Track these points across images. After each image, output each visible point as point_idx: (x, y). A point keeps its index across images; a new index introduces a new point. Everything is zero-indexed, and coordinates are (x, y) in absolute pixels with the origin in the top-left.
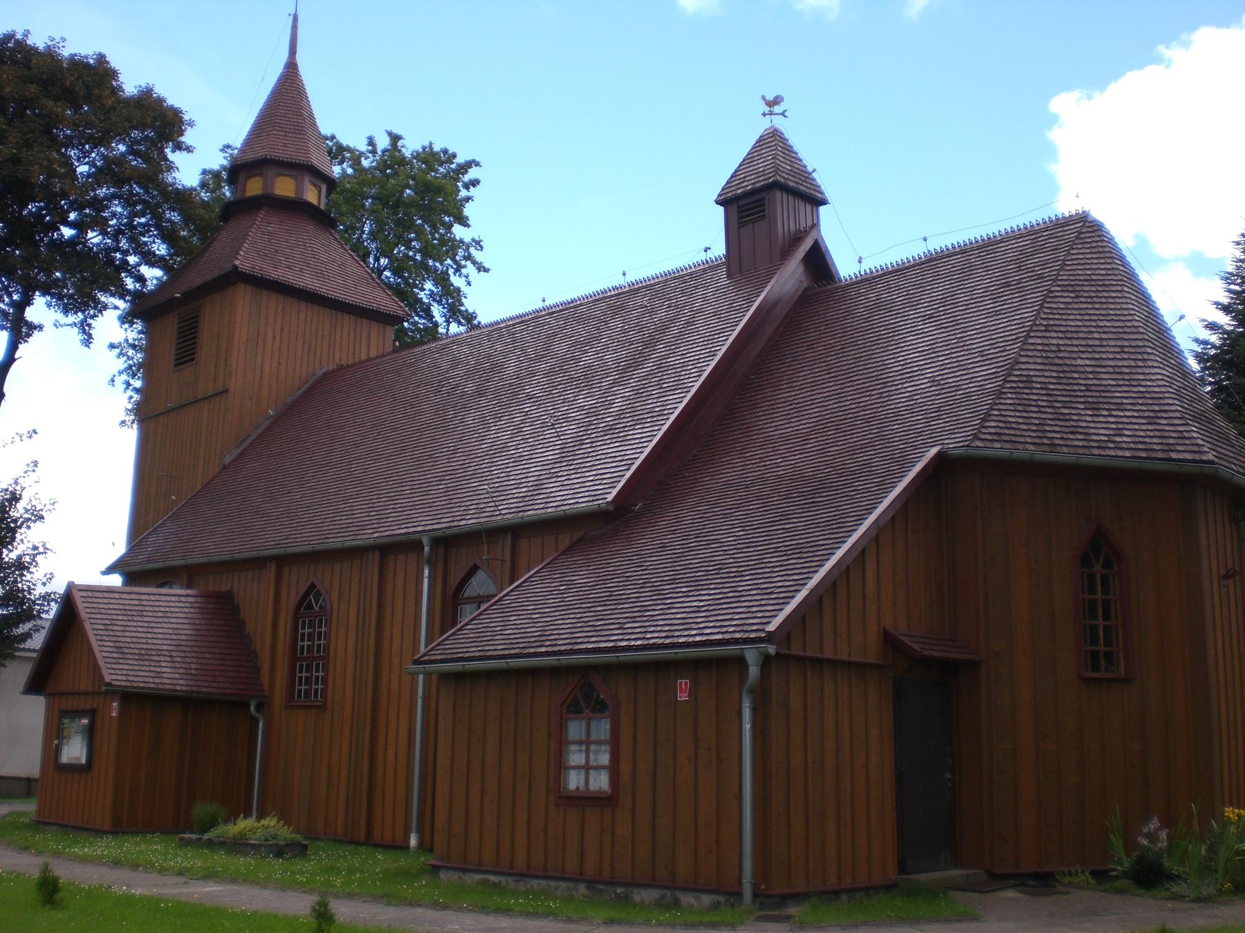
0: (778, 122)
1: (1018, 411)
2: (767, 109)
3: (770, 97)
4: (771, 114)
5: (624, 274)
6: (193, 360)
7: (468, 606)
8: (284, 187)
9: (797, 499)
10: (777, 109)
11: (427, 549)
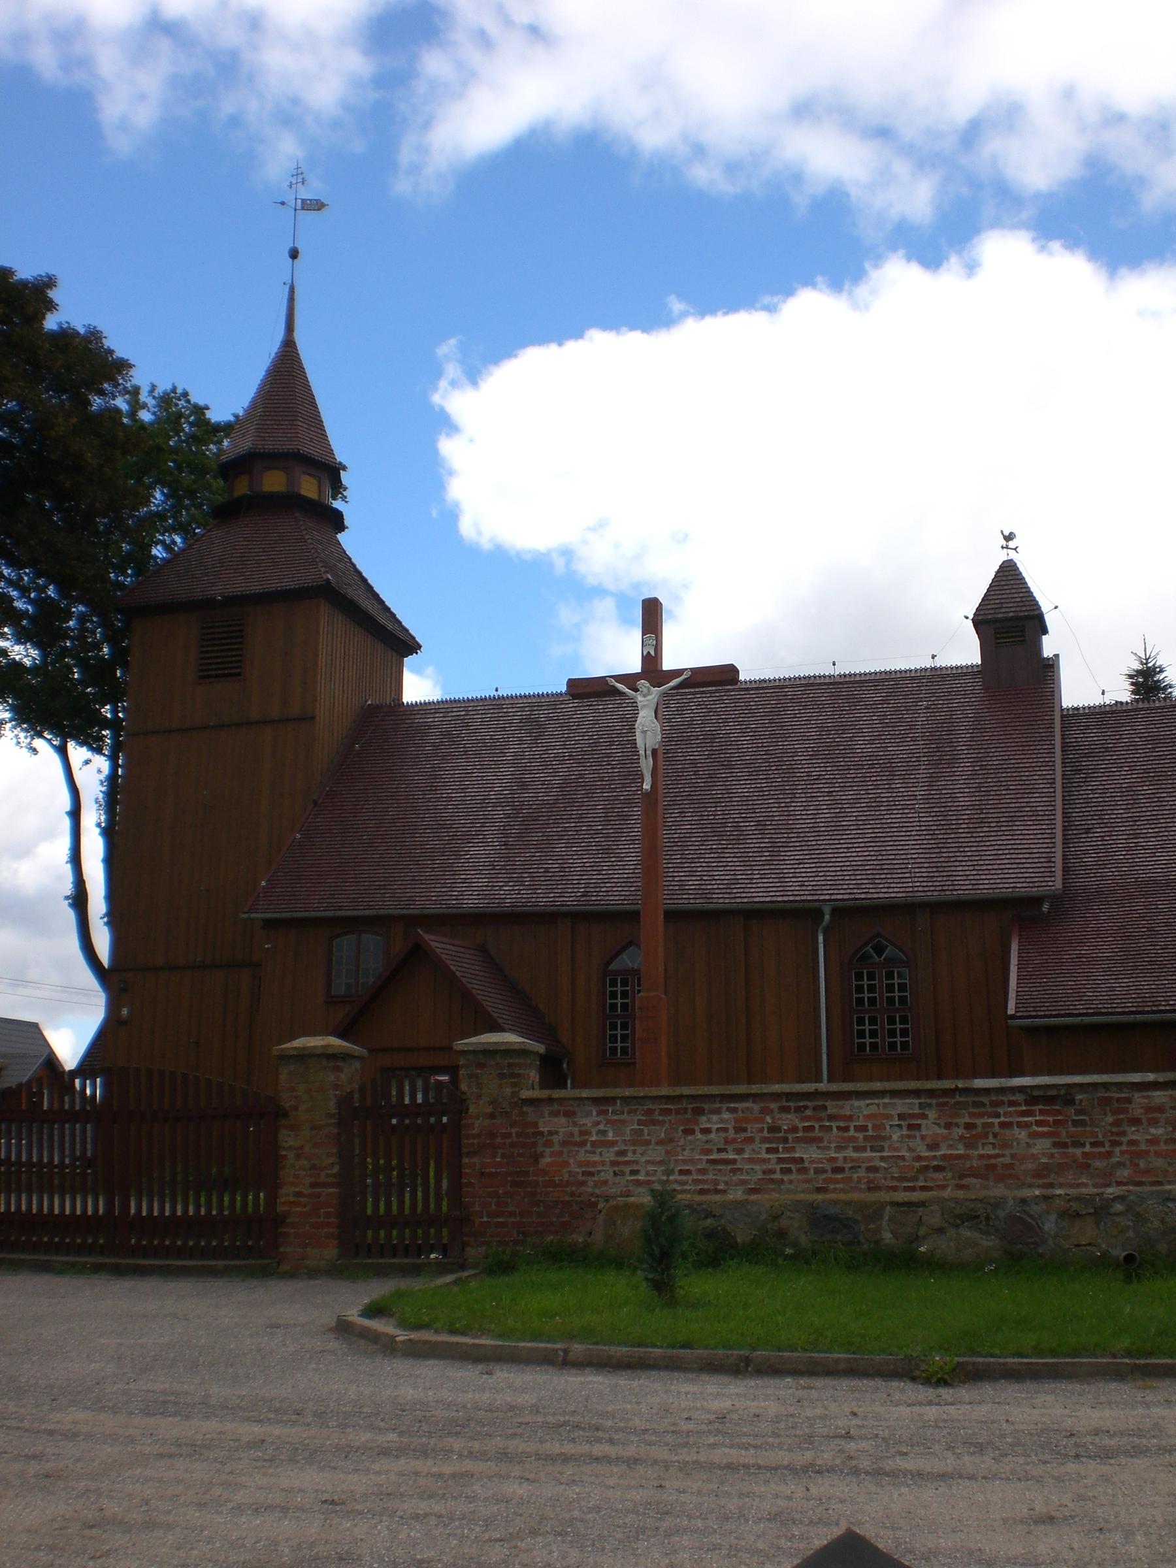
0: (1012, 555)
1: (1094, 819)
2: (1004, 543)
3: (1007, 533)
4: (1007, 547)
5: (834, 664)
6: (239, 674)
7: (343, 993)
8: (273, 482)
9: (771, 889)
10: (1012, 544)
11: (827, 917)
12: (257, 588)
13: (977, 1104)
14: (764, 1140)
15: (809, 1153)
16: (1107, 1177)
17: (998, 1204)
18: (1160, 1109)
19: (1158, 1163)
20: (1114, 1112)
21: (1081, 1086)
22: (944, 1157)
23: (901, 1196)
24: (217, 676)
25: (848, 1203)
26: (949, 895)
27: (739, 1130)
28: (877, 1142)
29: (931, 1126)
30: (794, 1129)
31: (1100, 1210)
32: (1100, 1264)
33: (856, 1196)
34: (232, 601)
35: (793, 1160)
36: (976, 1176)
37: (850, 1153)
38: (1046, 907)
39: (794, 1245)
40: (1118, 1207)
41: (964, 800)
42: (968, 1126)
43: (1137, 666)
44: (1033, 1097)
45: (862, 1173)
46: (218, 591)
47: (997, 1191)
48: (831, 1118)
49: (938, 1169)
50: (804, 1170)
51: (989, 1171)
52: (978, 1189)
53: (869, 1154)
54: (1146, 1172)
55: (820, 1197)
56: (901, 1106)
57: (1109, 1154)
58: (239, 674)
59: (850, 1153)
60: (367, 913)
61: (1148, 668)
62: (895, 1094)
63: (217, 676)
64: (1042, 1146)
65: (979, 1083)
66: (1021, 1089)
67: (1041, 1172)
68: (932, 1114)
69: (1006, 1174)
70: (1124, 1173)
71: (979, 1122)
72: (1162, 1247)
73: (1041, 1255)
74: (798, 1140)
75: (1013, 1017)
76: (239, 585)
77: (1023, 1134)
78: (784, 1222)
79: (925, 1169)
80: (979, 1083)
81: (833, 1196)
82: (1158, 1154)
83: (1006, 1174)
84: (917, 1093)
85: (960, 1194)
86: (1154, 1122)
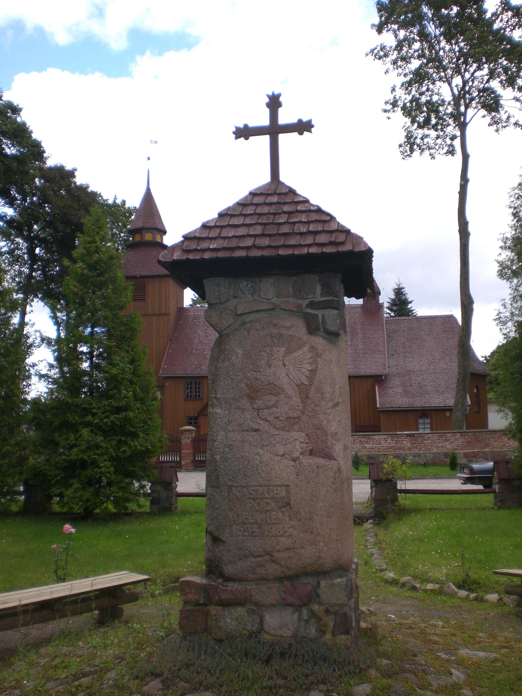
6: (144, 299)
12: (150, 274)
13: (398, 437)
14: (359, 443)
15: (367, 446)
16: (420, 450)
17: (401, 454)
18: (430, 438)
19: (429, 447)
20: (422, 438)
21: (416, 434)
22: (392, 446)
23: (384, 453)
24: (138, 300)
25: (374, 454)
26: (359, 374)
27: (354, 441)
28: (379, 443)
29: (389, 440)
30: (364, 441)
31: (419, 455)
32: (419, 465)
33: (376, 453)
34: (142, 277)
35: (364, 447)
36: (398, 449)
37: (375, 445)
38: (383, 377)
39: (365, 462)
40: (422, 455)
41: (360, 347)
42: (396, 441)
43: (396, 287)
44: (407, 435)
45: (377, 449)
46: (138, 273)
47: (401, 452)
48: (371, 439)
49: (390, 448)
50: (366, 449)
51: (399, 448)
52: (398, 452)
53: (378, 446)
54: (427, 449)
55: (369, 453)
56: (384, 437)
57: (421, 446)
58: (144, 299)
59: (375, 445)
60: (197, 375)
61: (400, 288)
62: (383, 435)
63: (138, 300)
64: (409, 444)
65: (398, 433)
66: (406, 434)
67: (409, 449)
68: (389, 438)
69: (402, 449)
70: (424, 449)
71: (398, 440)
72: (430, 462)
73: (126, 508)
74: (365, 443)
75: (379, 408)
76: (144, 273)
77: (406, 442)
78: (363, 458)
79: (388, 448)
80: (398, 433)
81: (372, 453)
82: (429, 446)
83: (402, 449)
84: (387, 435)
85: (395, 453)
86: (429, 440)
